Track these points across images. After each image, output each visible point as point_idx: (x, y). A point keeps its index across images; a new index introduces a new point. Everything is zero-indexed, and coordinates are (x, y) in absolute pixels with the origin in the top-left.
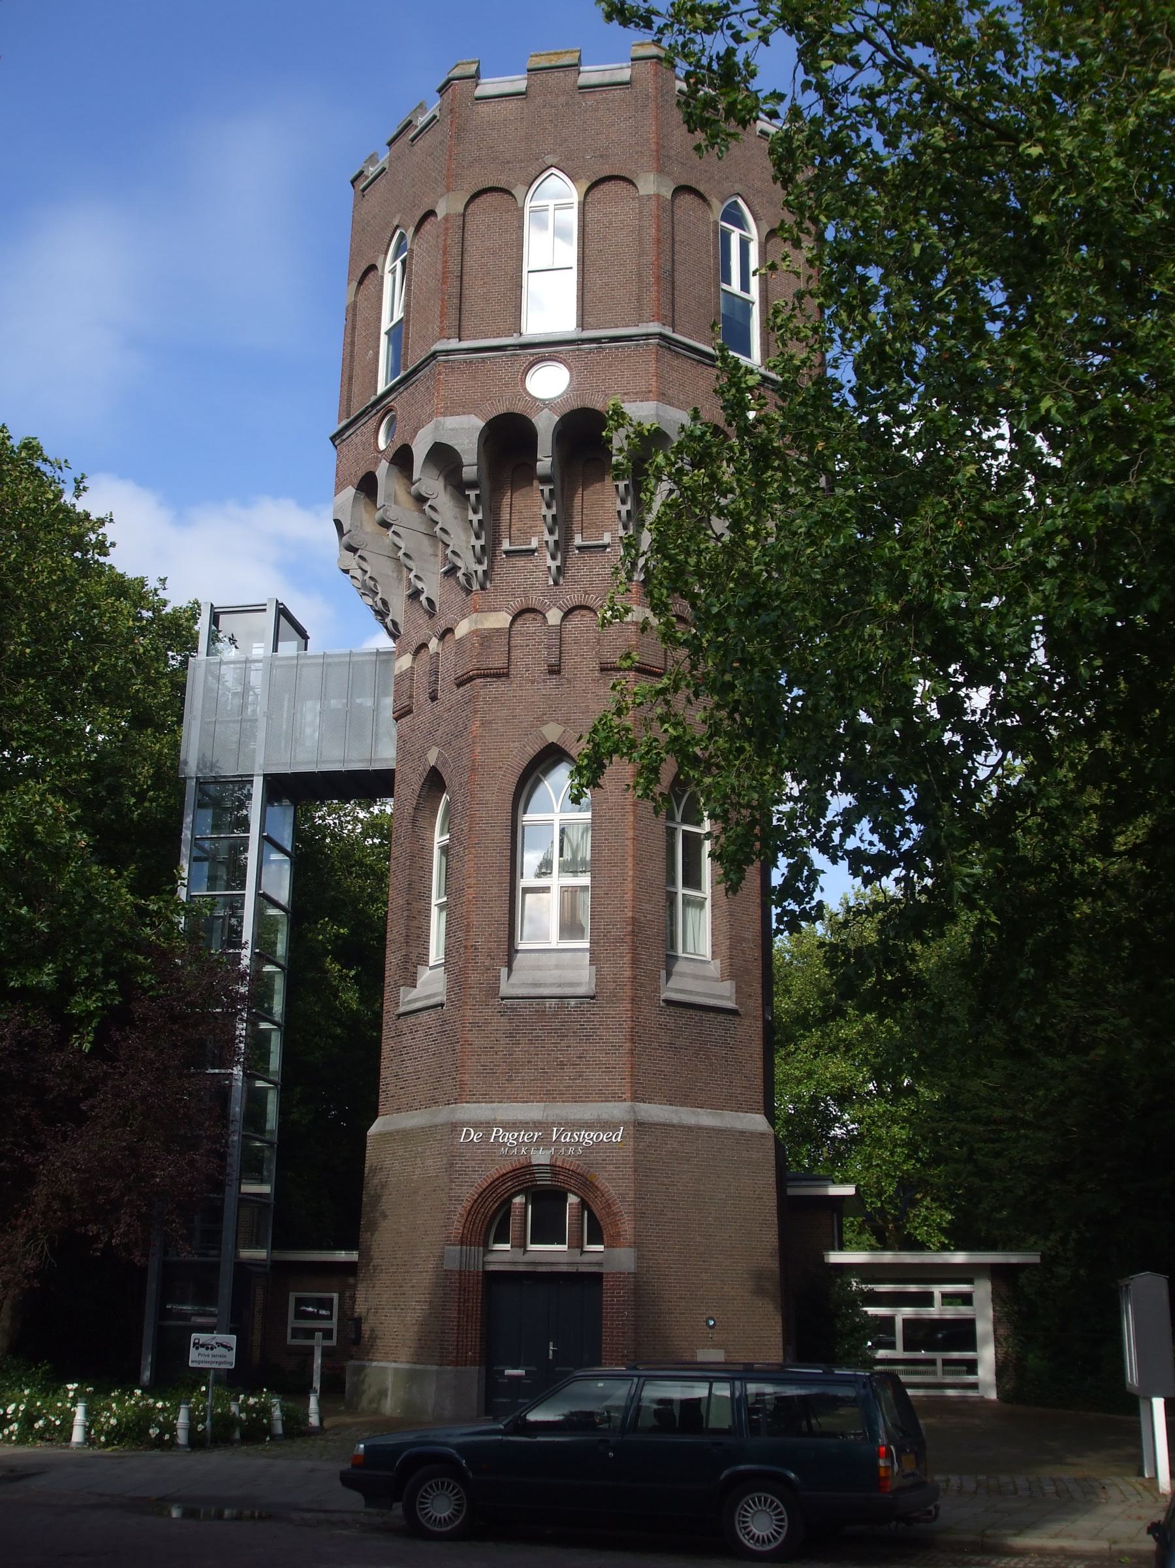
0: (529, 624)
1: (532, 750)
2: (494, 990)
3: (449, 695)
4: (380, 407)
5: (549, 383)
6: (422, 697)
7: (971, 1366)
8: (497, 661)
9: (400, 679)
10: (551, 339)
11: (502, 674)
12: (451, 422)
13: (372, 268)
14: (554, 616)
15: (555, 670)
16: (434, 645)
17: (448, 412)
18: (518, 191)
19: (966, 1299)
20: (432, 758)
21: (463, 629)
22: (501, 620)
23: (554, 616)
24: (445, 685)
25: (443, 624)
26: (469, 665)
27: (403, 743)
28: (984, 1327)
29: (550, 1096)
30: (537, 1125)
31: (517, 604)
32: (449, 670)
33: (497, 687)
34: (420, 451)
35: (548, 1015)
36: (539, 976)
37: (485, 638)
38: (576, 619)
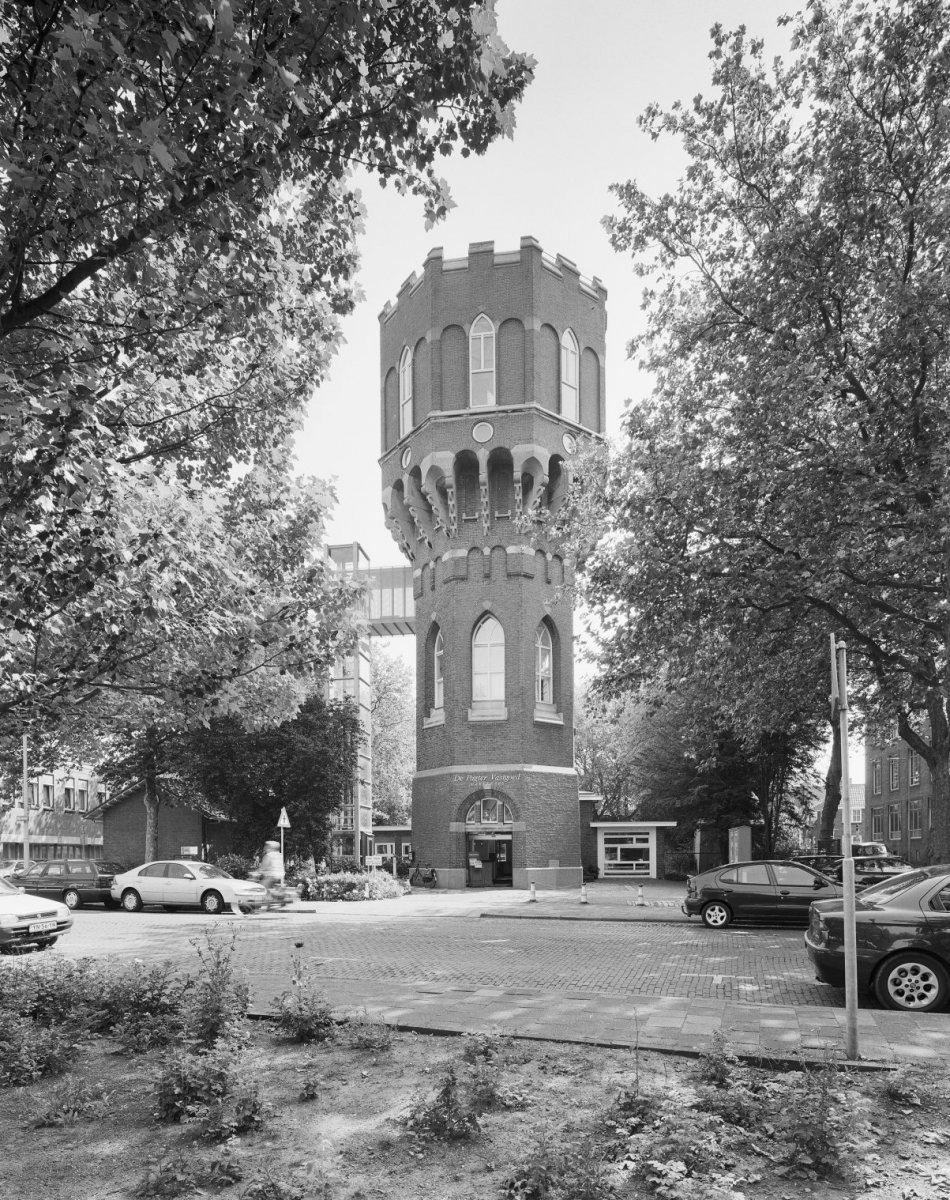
0: (476, 556)
1: (478, 614)
2: (465, 718)
3: (441, 589)
4: (403, 446)
5: (483, 434)
6: (427, 588)
7: (647, 867)
8: (462, 573)
9: (415, 581)
10: (385, 392)
11: (463, 579)
12: (440, 455)
13: (392, 368)
14: (487, 551)
15: (487, 576)
16: (432, 564)
17: (437, 449)
18: (465, 327)
19: (860, 907)
20: (433, 617)
21: (446, 557)
22: (463, 553)
23: (487, 551)
24: (439, 582)
25: (436, 554)
26: (449, 574)
27: (418, 609)
28: (653, 855)
29: (490, 762)
30: (485, 774)
31: (470, 545)
32: (441, 575)
33: (462, 585)
34: (424, 472)
35: (487, 728)
36: (485, 712)
37: (456, 562)
38: (496, 552)
